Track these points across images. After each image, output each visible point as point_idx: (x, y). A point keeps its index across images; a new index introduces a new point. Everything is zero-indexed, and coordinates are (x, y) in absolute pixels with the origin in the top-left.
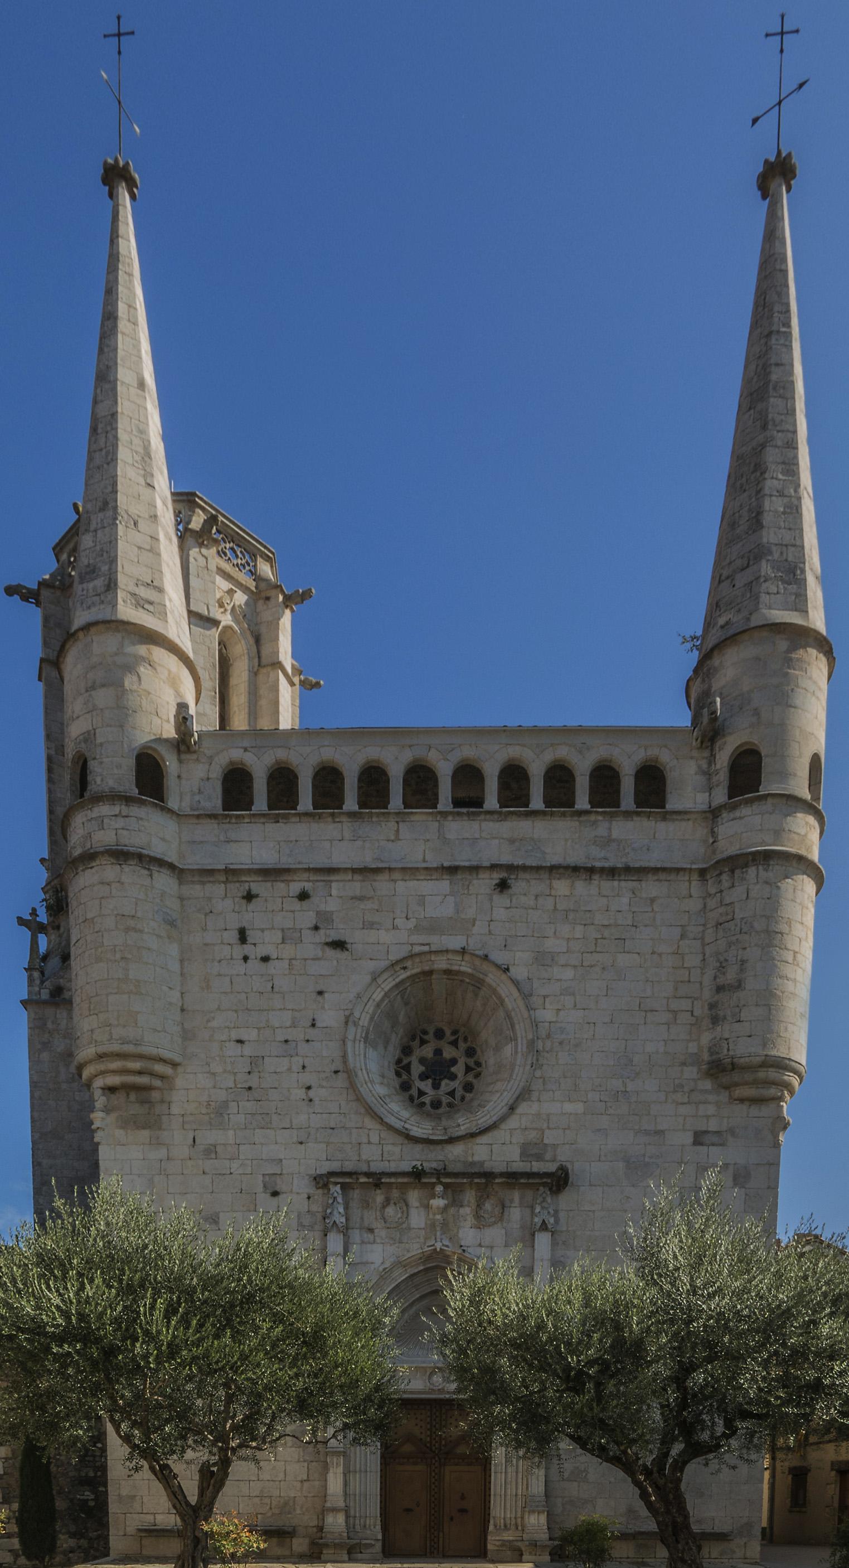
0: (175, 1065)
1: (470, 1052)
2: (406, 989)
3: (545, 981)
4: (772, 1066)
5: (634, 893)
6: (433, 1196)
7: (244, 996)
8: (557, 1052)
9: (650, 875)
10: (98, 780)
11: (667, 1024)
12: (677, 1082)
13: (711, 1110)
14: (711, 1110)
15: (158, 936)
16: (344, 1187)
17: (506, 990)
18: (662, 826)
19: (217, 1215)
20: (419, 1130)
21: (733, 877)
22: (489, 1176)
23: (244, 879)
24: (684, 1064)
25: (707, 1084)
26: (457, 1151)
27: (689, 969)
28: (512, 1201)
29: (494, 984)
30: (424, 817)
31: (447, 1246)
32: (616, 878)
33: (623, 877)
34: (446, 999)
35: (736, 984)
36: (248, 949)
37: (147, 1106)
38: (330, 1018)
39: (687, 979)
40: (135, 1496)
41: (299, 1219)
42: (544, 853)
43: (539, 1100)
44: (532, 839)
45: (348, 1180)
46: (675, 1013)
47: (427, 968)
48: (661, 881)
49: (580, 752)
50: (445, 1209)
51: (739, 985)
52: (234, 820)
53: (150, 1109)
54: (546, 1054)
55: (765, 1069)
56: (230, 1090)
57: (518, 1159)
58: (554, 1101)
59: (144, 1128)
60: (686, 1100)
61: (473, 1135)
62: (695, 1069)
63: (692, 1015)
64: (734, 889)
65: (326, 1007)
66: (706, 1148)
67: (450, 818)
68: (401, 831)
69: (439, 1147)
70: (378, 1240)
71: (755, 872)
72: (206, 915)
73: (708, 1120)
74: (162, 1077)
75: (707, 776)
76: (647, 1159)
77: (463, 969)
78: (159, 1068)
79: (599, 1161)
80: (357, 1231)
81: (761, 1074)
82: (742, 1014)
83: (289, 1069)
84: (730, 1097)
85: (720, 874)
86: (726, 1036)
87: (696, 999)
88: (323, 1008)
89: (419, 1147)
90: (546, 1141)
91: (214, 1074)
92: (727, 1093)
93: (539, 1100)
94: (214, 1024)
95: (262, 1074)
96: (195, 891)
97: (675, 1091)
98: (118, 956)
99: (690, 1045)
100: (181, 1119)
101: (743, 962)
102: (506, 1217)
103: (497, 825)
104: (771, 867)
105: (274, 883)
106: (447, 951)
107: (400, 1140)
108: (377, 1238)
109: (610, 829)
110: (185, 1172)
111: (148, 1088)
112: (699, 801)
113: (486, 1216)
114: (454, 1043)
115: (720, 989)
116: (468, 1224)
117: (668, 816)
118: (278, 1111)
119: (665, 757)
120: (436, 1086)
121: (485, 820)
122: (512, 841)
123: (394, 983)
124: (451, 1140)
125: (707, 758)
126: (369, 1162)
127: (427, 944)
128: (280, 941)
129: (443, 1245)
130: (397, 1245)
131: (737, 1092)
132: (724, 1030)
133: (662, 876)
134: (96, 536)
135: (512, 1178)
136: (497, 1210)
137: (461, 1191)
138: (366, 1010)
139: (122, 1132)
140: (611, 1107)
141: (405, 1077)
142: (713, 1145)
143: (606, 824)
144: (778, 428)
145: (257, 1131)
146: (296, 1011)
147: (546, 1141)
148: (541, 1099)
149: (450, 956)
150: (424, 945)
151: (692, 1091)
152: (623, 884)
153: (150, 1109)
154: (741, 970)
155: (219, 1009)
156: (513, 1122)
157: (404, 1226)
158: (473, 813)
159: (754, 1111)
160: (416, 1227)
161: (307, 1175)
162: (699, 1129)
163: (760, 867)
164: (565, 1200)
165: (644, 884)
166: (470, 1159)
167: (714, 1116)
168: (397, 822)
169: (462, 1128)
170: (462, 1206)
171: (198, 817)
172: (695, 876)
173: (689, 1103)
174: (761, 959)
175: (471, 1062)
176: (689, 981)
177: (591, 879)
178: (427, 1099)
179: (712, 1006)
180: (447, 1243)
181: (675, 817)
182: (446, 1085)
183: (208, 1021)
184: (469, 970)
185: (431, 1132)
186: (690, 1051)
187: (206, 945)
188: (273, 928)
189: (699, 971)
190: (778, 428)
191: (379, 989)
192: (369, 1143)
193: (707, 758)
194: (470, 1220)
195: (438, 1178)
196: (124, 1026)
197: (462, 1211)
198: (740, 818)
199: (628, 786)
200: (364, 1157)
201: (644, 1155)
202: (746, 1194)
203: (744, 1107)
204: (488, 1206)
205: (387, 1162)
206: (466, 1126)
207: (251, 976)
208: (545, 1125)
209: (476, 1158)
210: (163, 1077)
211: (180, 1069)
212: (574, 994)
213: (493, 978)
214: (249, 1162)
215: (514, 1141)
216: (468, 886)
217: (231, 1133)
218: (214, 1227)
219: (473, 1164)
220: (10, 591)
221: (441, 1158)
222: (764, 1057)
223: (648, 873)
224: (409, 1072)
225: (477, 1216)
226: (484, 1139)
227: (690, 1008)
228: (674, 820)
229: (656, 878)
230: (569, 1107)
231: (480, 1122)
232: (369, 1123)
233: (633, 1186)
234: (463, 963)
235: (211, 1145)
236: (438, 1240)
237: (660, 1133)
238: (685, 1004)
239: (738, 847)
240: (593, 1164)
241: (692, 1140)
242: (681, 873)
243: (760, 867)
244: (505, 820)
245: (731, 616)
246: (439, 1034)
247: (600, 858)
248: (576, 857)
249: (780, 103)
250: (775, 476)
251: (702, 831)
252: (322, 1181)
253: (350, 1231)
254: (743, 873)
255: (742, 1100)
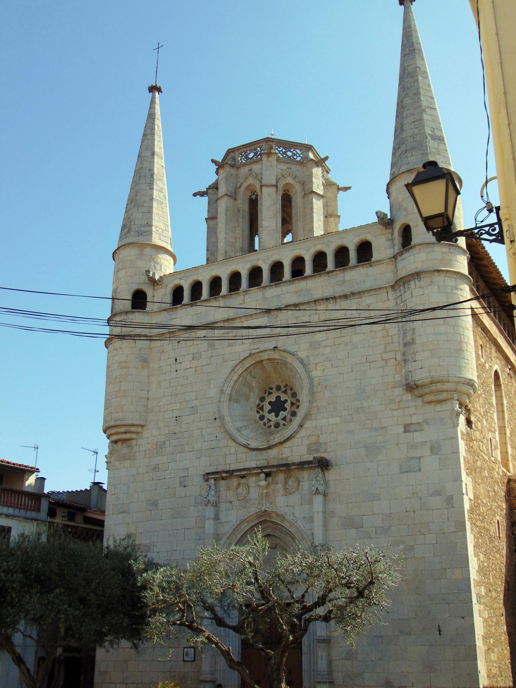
0: (143, 426)
1: (294, 395)
2: (251, 371)
3: (315, 356)
4: (438, 382)
5: (358, 304)
6: (260, 481)
7: (175, 387)
8: (324, 392)
9: (366, 294)
10: (117, 307)
11: (382, 367)
12: (391, 398)
13: (412, 411)
14: (412, 411)
15: (136, 368)
16: (215, 479)
17: (297, 365)
18: (370, 269)
19: (157, 501)
20: (255, 444)
21: (404, 287)
22: (287, 465)
23: (177, 334)
24: (394, 387)
25: (408, 396)
26: (273, 452)
27: (392, 336)
28: (303, 478)
29: (291, 362)
30: (256, 291)
31: (268, 508)
32: (349, 299)
33: (352, 298)
34: (275, 371)
35: (412, 341)
36: (178, 366)
37: (130, 448)
38: (213, 392)
39: (391, 342)
40: (107, 672)
41: (195, 499)
42: (312, 294)
43: (316, 419)
44: (306, 289)
45: (217, 476)
46: (386, 361)
47: (258, 360)
48: (372, 295)
49: (327, 245)
50: (267, 486)
51: (413, 342)
52: (174, 310)
53: (131, 450)
54: (318, 394)
55: (435, 385)
56: (167, 435)
57: (306, 453)
58: (323, 418)
59: (128, 460)
60: (397, 407)
61: (281, 443)
62: (401, 389)
63: (396, 360)
64: (406, 293)
65: (211, 387)
66: (411, 433)
67: (267, 288)
68: (245, 299)
69: (265, 452)
70: (234, 508)
71: (414, 283)
72: (161, 353)
73: (411, 417)
74: (137, 433)
75: (392, 241)
76: (378, 445)
77: (275, 357)
78: (133, 429)
79: (351, 449)
80: (224, 503)
81: (433, 387)
82: (416, 357)
83: (194, 421)
84: (423, 401)
85: (400, 287)
86: (410, 370)
87: (397, 351)
88: (210, 388)
89: (255, 453)
90: (320, 441)
91: (160, 428)
92: (420, 399)
93: (316, 419)
94: (161, 404)
95: (181, 425)
96: (154, 344)
97: (390, 403)
98: (117, 381)
99: (397, 376)
100: (144, 453)
101: (413, 329)
102: (300, 487)
103: (289, 287)
104: (422, 279)
105: (190, 334)
106: (266, 350)
107: (246, 450)
108: (234, 507)
109: (344, 276)
110: (144, 480)
111: (130, 440)
112: (390, 253)
113: (289, 488)
114: (285, 392)
115: (405, 345)
116: (281, 494)
117: (372, 264)
118: (188, 443)
119: (369, 238)
120: (277, 416)
121: (284, 286)
122: (297, 292)
123: (243, 370)
124: (270, 448)
125: (390, 233)
126: (230, 464)
127: (258, 348)
128: (192, 359)
129: (266, 508)
130: (244, 509)
131: (425, 399)
132: (410, 366)
133: (372, 293)
134: (128, 213)
135: (302, 465)
136: (296, 485)
137: (277, 475)
138: (229, 386)
139: (118, 463)
140: (355, 417)
141: (261, 413)
142: (416, 431)
143: (342, 275)
144: (410, 89)
145: (178, 454)
146: (198, 391)
147: (320, 441)
148: (317, 418)
149: (269, 352)
150: (256, 349)
151: (400, 401)
152: (352, 301)
153: (131, 450)
154: (413, 334)
155: (163, 396)
156: (303, 433)
157: (247, 498)
158: (278, 284)
159: (438, 407)
160: (253, 498)
161: (200, 475)
162: (406, 423)
163: (416, 280)
164: (331, 475)
165: (363, 298)
166: (281, 457)
167: (415, 414)
168: (244, 295)
169: (276, 440)
170: (277, 484)
171: (160, 311)
172: (390, 290)
173: (399, 409)
174: (422, 326)
175: (294, 400)
176: (392, 343)
177: (336, 302)
178: (272, 424)
179: (404, 354)
180: (268, 506)
181: (376, 263)
182: (282, 414)
183: (159, 402)
184: (278, 357)
185: (260, 444)
186: (397, 379)
187: (160, 367)
188: (189, 354)
189: (397, 336)
190: (410, 89)
191: (236, 374)
192: (230, 454)
193: (390, 233)
194: (282, 491)
195: (261, 470)
196: (117, 413)
197: (277, 486)
198: (405, 259)
199: (353, 255)
200: (228, 462)
201: (376, 442)
202: (440, 459)
203: (432, 406)
204: (290, 482)
205: (239, 463)
206: (278, 438)
207: (178, 378)
208: (320, 433)
209: (284, 456)
210: (137, 433)
211: (145, 428)
212: (331, 360)
213: (290, 359)
214: (173, 471)
215: (304, 443)
216: (276, 318)
217: (166, 457)
218: (155, 508)
219: (282, 459)
220: (195, 195)
221: (266, 458)
222: (431, 379)
223: (364, 293)
224: (262, 410)
225: (285, 489)
226: (286, 445)
227: (394, 357)
228: (375, 265)
229: (369, 294)
230: (332, 421)
231: (285, 436)
232: (231, 443)
233: (371, 461)
234: (275, 354)
235: (157, 464)
236: (264, 505)
237: (383, 428)
238: (392, 355)
239: (405, 273)
240: (347, 451)
241: (403, 430)
242: (382, 290)
243: (416, 280)
244: (293, 284)
245: (395, 169)
246: (278, 388)
247: (339, 291)
248: (328, 293)
249: (158, 48)
250: (409, 108)
251: (391, 267)
252: (207, 476)
253: (220, 504)
254: (408, 284)
255: (430, 403)
